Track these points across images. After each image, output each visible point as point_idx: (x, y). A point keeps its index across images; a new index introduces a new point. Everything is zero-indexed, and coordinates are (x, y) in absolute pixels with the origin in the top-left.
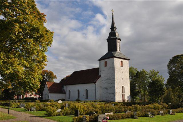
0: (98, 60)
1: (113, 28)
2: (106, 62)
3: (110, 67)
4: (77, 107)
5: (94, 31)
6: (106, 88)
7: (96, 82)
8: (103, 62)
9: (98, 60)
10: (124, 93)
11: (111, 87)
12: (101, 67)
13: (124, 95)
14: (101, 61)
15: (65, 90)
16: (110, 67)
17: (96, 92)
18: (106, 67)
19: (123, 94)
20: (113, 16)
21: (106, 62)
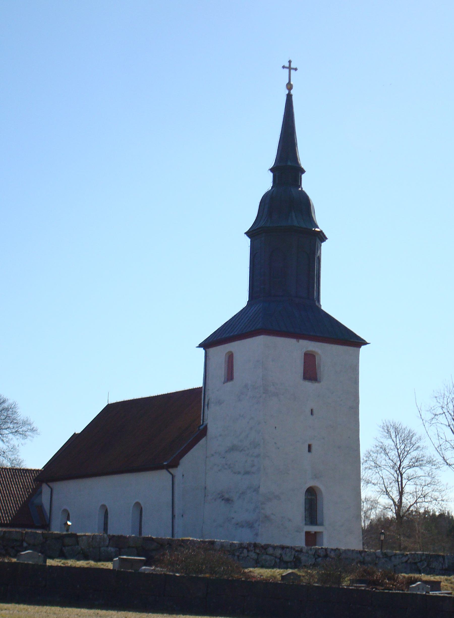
0: (200, 346)
1: (287, 168)
2: (230, 358)
3: (246, 386)
4: (413, 439)
5: (27, 420)
6: (226, 496)
7: (175, 464)
8: (220, 352)
9: (200, 346)
10: (322, 524)
11: (243, 493)
12: (209, 387)
13: (321, 533)
14: (212, 350)
15: (46, 507)
16: (246, 386)
17: (173, 516)
18: (229, 384)
19: (313, 529)
20: (289, 98)
21: (230, 358)
